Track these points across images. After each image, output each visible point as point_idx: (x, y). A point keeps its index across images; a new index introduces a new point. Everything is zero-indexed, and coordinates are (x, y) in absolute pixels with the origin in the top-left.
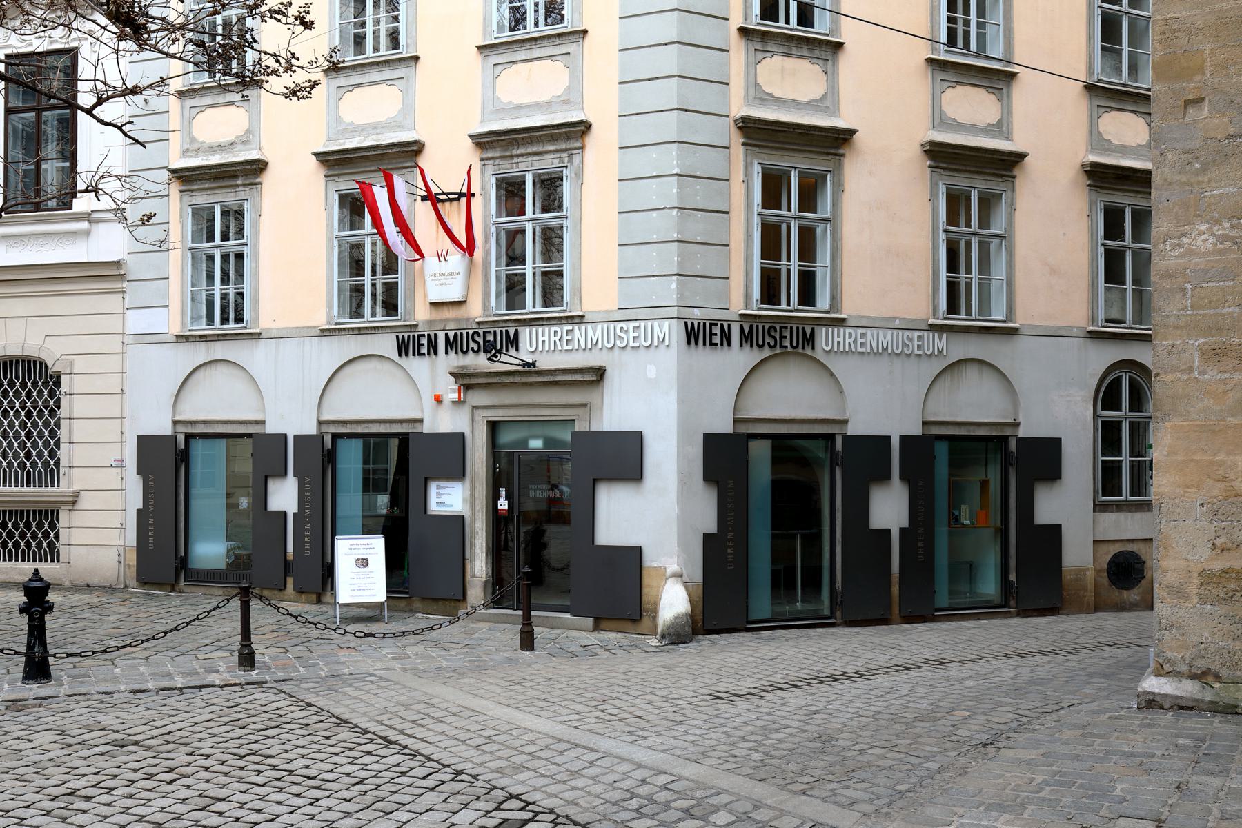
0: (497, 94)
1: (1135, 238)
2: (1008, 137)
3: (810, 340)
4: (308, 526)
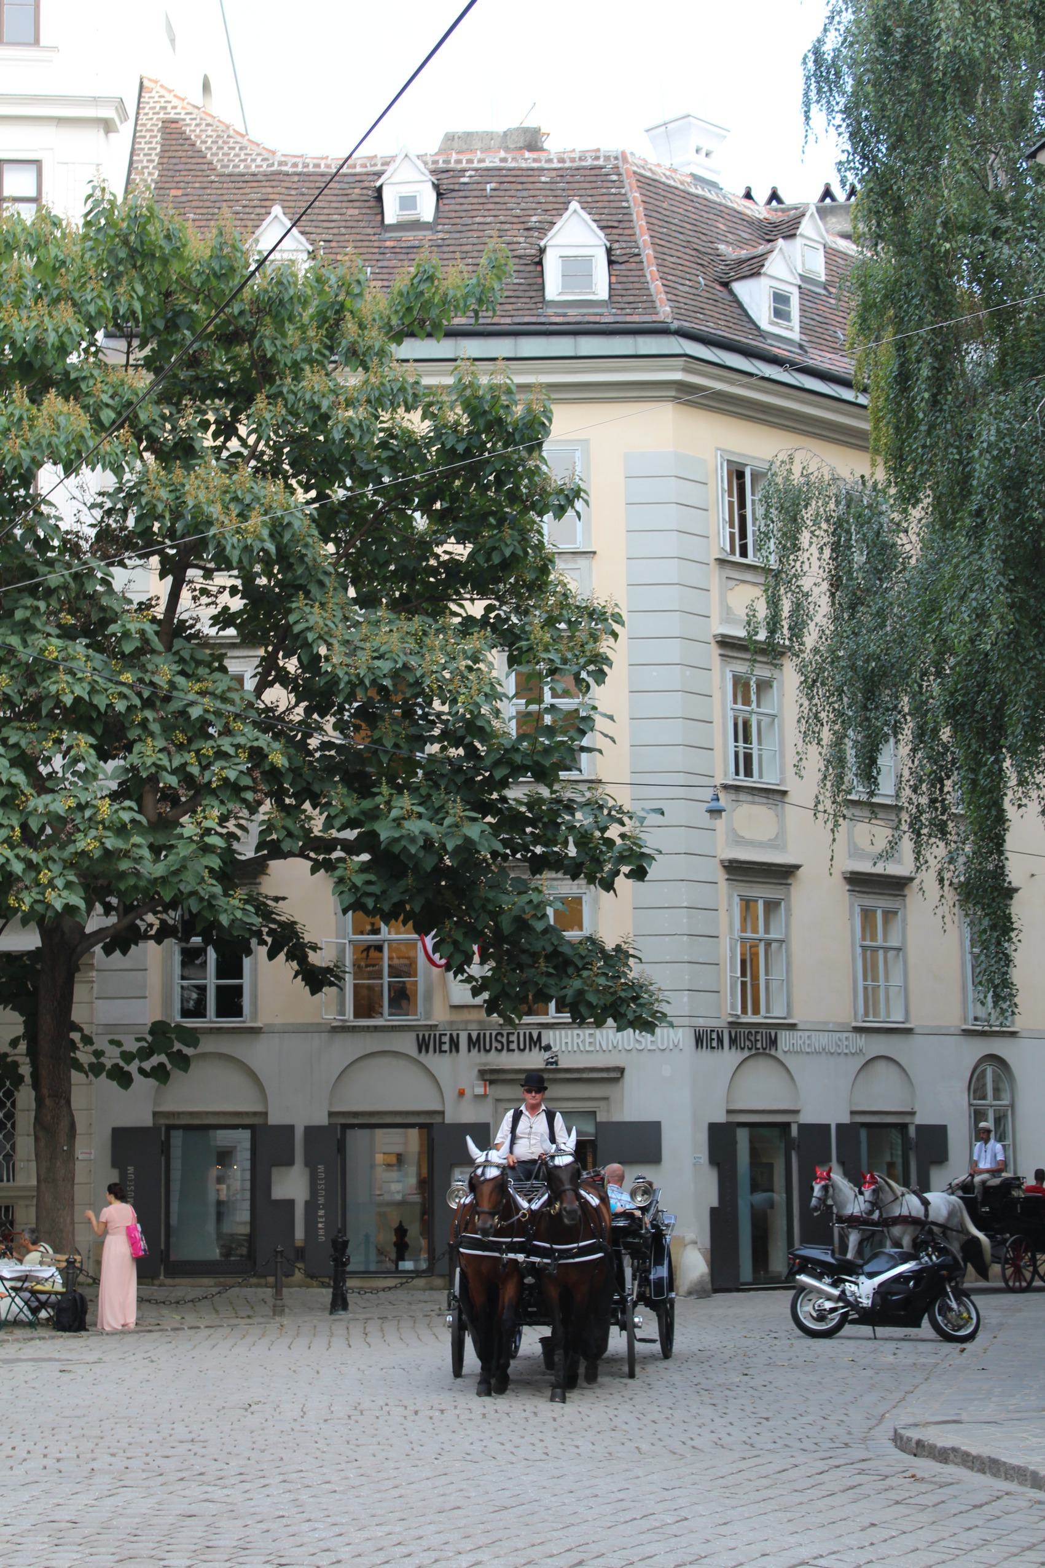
3: (774, 1042)
4: (321, 1213)
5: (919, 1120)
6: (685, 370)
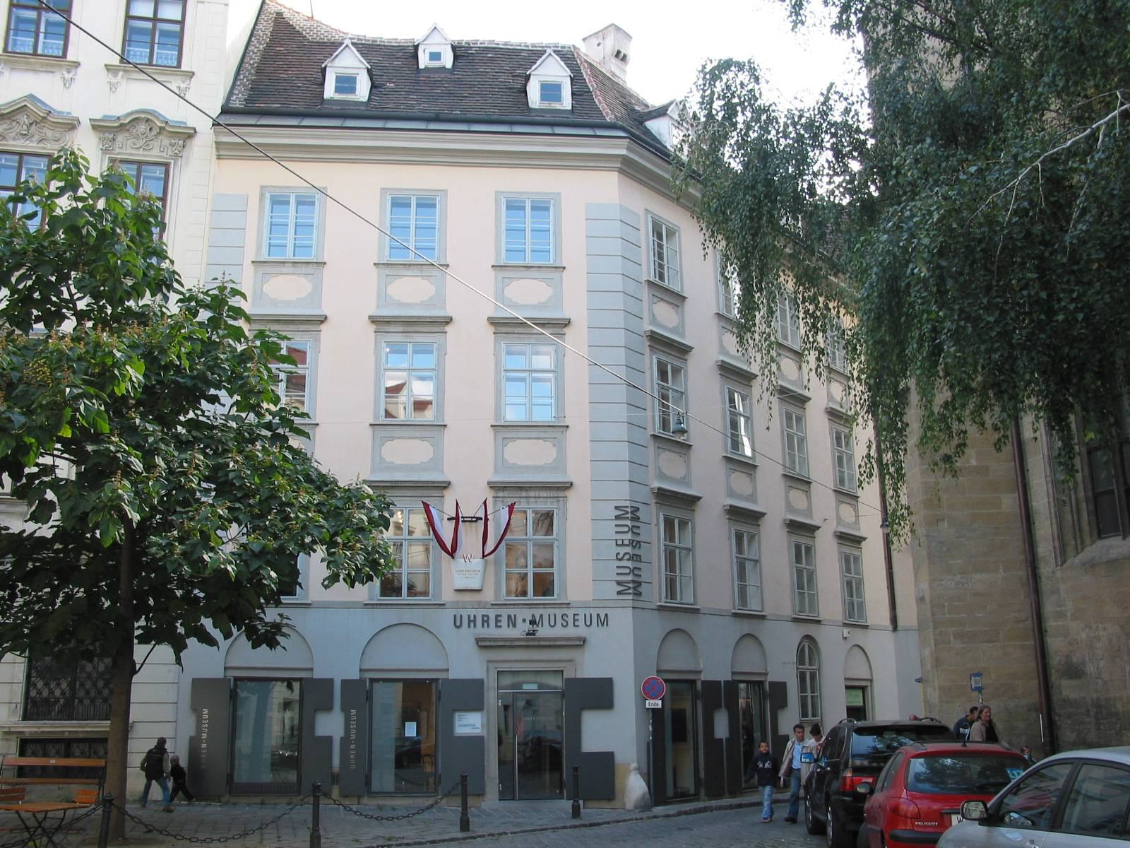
0: (505, 456)
1: (807, 564)
2: (689, 485)
4: (353, 746)
5: (703, 677)
6: (628, 149)
